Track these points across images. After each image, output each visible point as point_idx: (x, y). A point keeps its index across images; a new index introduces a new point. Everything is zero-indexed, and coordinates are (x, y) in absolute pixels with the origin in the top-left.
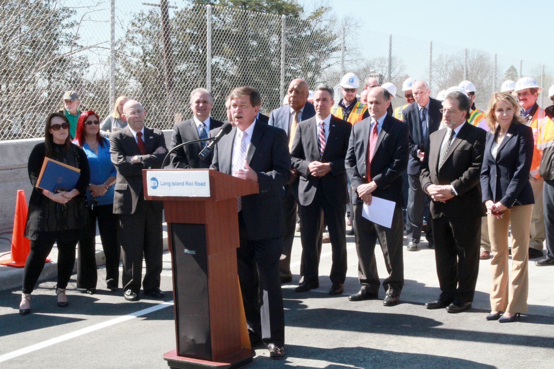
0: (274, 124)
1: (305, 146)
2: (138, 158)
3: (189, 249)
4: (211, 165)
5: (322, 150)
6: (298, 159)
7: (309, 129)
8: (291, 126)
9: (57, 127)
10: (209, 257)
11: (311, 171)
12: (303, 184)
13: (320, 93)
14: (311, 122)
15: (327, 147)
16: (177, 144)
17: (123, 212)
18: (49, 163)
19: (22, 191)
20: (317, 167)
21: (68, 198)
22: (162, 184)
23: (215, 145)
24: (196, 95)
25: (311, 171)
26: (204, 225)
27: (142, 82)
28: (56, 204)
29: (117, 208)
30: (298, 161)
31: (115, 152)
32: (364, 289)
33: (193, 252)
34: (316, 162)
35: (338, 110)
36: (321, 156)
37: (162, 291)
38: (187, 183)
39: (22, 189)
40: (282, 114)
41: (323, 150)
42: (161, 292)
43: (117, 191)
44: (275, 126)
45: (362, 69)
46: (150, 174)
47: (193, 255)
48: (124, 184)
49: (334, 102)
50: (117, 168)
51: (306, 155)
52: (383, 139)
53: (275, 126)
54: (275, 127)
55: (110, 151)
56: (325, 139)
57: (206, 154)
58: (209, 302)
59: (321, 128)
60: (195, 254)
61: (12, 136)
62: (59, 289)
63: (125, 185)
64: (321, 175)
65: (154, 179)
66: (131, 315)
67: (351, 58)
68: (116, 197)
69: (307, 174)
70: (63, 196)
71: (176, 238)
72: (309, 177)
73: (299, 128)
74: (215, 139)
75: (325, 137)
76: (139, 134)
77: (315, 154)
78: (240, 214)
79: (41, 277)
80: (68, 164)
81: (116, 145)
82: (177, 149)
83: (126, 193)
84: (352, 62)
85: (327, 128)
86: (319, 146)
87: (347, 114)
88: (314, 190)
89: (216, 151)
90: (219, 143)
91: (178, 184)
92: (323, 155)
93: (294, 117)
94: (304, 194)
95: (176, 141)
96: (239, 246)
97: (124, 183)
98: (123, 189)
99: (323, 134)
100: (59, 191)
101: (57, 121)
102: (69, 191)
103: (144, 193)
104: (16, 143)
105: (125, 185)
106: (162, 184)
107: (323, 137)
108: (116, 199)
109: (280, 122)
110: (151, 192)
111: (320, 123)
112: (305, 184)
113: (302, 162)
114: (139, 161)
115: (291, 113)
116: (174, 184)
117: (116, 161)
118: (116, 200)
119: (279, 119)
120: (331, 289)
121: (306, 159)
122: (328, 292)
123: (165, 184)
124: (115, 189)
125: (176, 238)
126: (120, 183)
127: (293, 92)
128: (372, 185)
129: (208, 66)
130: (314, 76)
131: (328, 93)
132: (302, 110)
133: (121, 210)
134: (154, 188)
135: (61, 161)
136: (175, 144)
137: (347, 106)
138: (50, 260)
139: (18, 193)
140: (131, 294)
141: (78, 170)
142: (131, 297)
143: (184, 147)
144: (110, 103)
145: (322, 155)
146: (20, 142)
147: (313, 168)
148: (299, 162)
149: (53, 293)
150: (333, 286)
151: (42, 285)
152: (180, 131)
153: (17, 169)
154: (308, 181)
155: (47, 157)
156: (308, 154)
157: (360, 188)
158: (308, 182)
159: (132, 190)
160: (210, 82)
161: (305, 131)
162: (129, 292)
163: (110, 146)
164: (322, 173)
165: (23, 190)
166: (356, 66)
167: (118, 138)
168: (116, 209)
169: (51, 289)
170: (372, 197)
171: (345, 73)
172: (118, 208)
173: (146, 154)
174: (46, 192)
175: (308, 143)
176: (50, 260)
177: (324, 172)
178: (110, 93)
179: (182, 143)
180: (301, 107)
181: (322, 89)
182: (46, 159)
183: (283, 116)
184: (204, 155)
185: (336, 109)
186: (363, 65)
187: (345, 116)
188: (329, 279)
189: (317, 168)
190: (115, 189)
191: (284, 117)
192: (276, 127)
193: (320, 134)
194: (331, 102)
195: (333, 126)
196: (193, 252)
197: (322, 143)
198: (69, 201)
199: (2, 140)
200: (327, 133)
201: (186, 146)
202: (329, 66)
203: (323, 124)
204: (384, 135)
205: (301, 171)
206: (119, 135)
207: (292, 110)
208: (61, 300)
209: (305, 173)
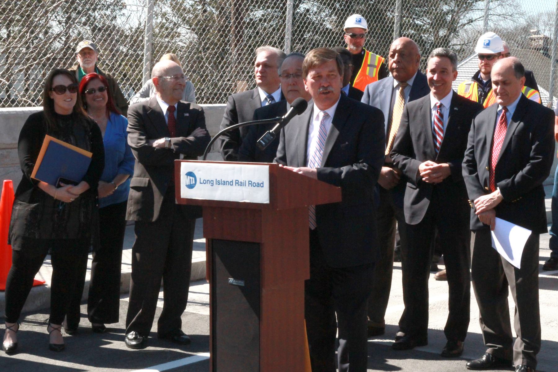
0: (369, 102)
1: (414, 139)
2: (166, 141)
3: (235, 278)
4: (275, 158)
5: (438, 144)
6: (403, 157)
7: (419, 114)
8: (393, 106)
9: (61, 89)
10: (264, 292)
11: (421, 174)
12: (410, 193)
13: (437, 61)
14: (424, 103)
15: (445, 139)
16: (231, 124)
17: (140, 219)
18: (51, 143)
19: (10, 182)
20: (430, 169)
21: (75, 195)
22: (202, 182)
23: (282, 130)
24: (262, 55)
25: (421, 174)
26: (259, 244)
27: (196, 33)
28: (57, 202)
29: (131, 212)
30: (404, 159)
31: (134, 130)
32: (490, 353)
33: (242, 283)
34: (429, 162)
35: (471, 87)
36: (436, 153)
37: (186, 335)
38: (237, 182)
39: (10, 179)
40: (382, 89)
41: (440, 143)
42: (184, 336)
43: (133, 188)
44: (370, 104)
45: (520, 28)
46: (185, 166)
47: (240, 287)
48: (145, 178)
49: (457, 73)
50: (134, 153)
51: (416, 151)
52: (514, 133)
53: (370, 104)
54: (370, 106)
55: (128, 130)
56: (442, 128)
57: (267, 142)
58: (260, 358)
59: (438, 112)
60: (243, 285)
61: (10, 102)
62: (53, 325)
63: (145, 181)
64: (436, 181)
65: (190, 174)
66: (148, 369)
67: (504, 11)
68: (132, 196)
69: (417, 179)
70: (68, 192)
71: (218, 260)
72: (419, 183)
73: (406, 112)
74: (282, 120)
75: (443, 125)
76: (170, 109)
77: (428, 151)
78: (313, 234)
79: (25, 309)
80: (77, 145)
81: (137, 122)
82: (231, 130)
83: (146, 191)
84: (505, 16)
85: (446, 113)
86: (435, 138)
87: (483, 91)
88: (425, 202)
89: (283, 138)
90: (286, 127)
91: (225, 183)
92: (440, 152)
93: (398, 92)
94: (411, 208)
95: (230, 119)
96: (308, 278)
97: (144, 177)
98: (142, 185)
99: (439, 120)
100: (62, 184)
101: (60, 81)
102: (76, 184)
103: (176, 195)
104: (7, 113)
105: (145, 181)
106: (202, 182)
107: (440, 125)
108: (131, 199)
109: (378, 99)
110: (185, 193)
111: (436, 105)
112: (412, 193)
113: (410, 161)
114: (167, 146)
115: (395, 87)
116: (219, 183)
117: (134, 144)
118: (131, 201)
119: (377, 95)
120: (445, 348)
121: (417, 157)
122: (440, 353)
123: (205, 182)
124: (131, 185)
125: (218, 260)
126: (138, 177)
127: (397, 54)
128: (494, 196)
129: (289, 14)
130: (448, 36)
131: (449, 61)
132: (411, 82)
133: (137, 215)
134: (191, 186)
135: (67, 141)
136: (228, 123)
137: (485, 81)
138: (44, 282)
139: (4, 184)
140: (135, 339)
141: (89, 154)
142: (134, 343)
143: (240, 128)
144: (144, 61)
145: (438, 152)
146: (14, 111)
147: (425, 170)
148: (405, 162)
149: (44, 330)
150: (448, 344)
151: (30, 317)
152: (236, 105)
153: (7, 150)
154: (418, 190)
155: (48, 135)
156: (418, 150)
157: (478, 201)
158: (418, 190)
159: (154, 187)
160: (290, 38)
161: (415, 116)
162: (133, 334)
163: (127, 124)
164: (438, 178)
165: (11, 181)
166: (511, 23)
167: (141, 111)
168: (130, 214)
169: (41, 324)
170: (495, 218)
171: (486, 30)
172: (134, 212)
173: (179, 136)
174: (44, 185)
175: (418, 132)
176: (44, 282)
177: (440, 176)
178: (145, 47)
179: (238, 123)
180: (409, 78)
181: (439, 55)
182: (48, 139)
183: (383, 91)
184: (264, 144)
185: (470, 84)
186: (522, 22)
187: (481, 94)
188: (444, 334)
189: (430, 171)
190: (131, 185)
191: (384, 92)
192: (373, 105)
193: (436, 120)
194: (452, 75)
195: (455, 109)
196: (242, 283)
197: (439, 135)
198: (76, 199)
199: (3, 106)
200: (446, 120)
201: (243, 127)
202: (472, 21)
203: (441, 106)
204: (517, 126)
205: (408, 174)
206: (142, 108)
207: (396, 83)
208: (53, 341)
209: (414, 178)
